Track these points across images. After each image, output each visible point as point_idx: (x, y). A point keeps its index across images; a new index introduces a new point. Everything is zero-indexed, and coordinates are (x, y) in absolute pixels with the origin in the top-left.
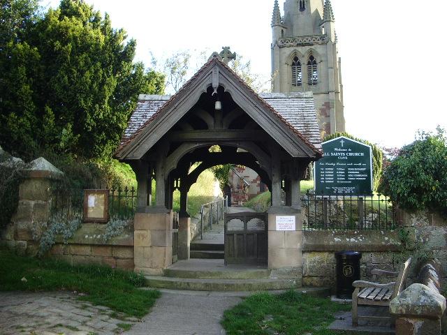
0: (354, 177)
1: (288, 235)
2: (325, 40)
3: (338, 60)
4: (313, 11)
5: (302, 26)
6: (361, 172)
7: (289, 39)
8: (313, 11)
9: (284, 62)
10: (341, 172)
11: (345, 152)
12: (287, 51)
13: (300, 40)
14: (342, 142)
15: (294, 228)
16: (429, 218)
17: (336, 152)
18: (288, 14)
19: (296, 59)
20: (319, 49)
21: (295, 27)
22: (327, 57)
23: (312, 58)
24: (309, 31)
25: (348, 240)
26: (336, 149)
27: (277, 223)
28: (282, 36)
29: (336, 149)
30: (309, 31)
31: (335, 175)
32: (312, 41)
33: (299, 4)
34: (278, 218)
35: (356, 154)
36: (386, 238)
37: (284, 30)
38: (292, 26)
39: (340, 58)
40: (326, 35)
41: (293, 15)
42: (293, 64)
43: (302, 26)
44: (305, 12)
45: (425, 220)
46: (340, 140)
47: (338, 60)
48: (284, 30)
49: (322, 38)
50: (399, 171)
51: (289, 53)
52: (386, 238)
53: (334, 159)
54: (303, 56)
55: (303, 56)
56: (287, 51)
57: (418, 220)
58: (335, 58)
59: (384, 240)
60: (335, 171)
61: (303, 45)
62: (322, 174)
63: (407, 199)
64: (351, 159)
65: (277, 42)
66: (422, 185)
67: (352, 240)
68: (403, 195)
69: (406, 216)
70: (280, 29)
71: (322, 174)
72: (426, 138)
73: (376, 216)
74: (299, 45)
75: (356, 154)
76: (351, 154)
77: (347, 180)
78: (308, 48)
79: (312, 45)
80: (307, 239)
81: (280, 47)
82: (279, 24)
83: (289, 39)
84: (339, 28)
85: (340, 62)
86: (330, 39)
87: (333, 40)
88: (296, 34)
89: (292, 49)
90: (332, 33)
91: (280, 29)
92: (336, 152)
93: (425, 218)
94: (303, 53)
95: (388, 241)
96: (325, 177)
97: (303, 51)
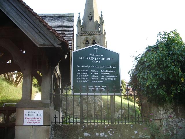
0: (105, 78)
1: (36, 130)
2: (100, 33)
3: (106, 42)
4: (95, 20)
5: (90, 27)
6: (112, 74)
7: (84, 32)
8: (95, 20)
9: (82, 42)
10: (95, 73)
11: (99, 57)
12: (83, 38)
13: (89, 33)
14: (96, 49)
15: (41, 123)
16: (175, 110)
17: (91, 57)
18: (84, 22)
19: (87, 41)
20: (98, 37)
21: (87, 27)
22: (101, 40)
23: (94, 41)
24: (93, 29)
25: (97, 134)
26: (91, 55)
27: (25, 117)
28: (81, 30)
29: (91, 55)
30: (93, 29)
31: (90, 75)
32: (94, 33)
33: (89, 17)
34: (26, 112)
35: (108, 59)
36: (136, 132)
37: (82, 28)
38: (86, 27)
39: (107, 42)
40: (101, 31)
41: (86, 22)
42: (86, 43)
43: (90, 27)
44: (92, 20)
45: (172, 112)
46: (95, 47)
47: (106, 42)
48: (82, 28)
49: (99, 32)
50: (147, 64)
51: (84, 38)
52: (136, 132)
53: (90, 63)
54: (90, 40)
55: (90, 40)
56: (83, 38)
57: (166, 113)
58: (104, 41)
59: (134, 134)
60: (90, 72)
61: (90, 35)
62: (79, 75)
63: (156, 92)
64: (103, 63)
65: (79, 33)
66: (171, 77)
67: (102, 134)
68: (153, 88)
69: (154, 110)
70: (81, 28)
71: (79, 75)
72: (167, 38)
73: (123, 111)
74: (88, 35)
75: (108, 59)
76: (103, 59)
77: (99, 80)
78: (92, 36)
79: (94, 35)
80: (56, 133)
81: (80, 36)
82: (80, 25)
83: (84, 32)
84: (106, 28)
85: (107, 43)
86: (102, 32)
87: (104, 33)
88: (87, 30)
89: (86, 36)
90: (104, 30)
91: (81, 28)
92: (91, 57)
93: (171, 110)
94: (90, 39)
95: (137, 135)
96: (81, 77)
97: (90, 37)
